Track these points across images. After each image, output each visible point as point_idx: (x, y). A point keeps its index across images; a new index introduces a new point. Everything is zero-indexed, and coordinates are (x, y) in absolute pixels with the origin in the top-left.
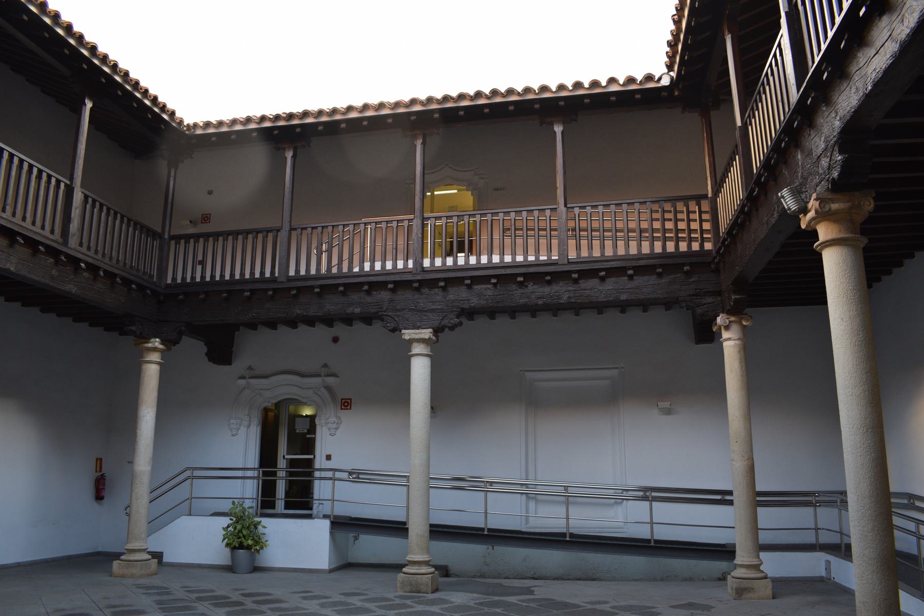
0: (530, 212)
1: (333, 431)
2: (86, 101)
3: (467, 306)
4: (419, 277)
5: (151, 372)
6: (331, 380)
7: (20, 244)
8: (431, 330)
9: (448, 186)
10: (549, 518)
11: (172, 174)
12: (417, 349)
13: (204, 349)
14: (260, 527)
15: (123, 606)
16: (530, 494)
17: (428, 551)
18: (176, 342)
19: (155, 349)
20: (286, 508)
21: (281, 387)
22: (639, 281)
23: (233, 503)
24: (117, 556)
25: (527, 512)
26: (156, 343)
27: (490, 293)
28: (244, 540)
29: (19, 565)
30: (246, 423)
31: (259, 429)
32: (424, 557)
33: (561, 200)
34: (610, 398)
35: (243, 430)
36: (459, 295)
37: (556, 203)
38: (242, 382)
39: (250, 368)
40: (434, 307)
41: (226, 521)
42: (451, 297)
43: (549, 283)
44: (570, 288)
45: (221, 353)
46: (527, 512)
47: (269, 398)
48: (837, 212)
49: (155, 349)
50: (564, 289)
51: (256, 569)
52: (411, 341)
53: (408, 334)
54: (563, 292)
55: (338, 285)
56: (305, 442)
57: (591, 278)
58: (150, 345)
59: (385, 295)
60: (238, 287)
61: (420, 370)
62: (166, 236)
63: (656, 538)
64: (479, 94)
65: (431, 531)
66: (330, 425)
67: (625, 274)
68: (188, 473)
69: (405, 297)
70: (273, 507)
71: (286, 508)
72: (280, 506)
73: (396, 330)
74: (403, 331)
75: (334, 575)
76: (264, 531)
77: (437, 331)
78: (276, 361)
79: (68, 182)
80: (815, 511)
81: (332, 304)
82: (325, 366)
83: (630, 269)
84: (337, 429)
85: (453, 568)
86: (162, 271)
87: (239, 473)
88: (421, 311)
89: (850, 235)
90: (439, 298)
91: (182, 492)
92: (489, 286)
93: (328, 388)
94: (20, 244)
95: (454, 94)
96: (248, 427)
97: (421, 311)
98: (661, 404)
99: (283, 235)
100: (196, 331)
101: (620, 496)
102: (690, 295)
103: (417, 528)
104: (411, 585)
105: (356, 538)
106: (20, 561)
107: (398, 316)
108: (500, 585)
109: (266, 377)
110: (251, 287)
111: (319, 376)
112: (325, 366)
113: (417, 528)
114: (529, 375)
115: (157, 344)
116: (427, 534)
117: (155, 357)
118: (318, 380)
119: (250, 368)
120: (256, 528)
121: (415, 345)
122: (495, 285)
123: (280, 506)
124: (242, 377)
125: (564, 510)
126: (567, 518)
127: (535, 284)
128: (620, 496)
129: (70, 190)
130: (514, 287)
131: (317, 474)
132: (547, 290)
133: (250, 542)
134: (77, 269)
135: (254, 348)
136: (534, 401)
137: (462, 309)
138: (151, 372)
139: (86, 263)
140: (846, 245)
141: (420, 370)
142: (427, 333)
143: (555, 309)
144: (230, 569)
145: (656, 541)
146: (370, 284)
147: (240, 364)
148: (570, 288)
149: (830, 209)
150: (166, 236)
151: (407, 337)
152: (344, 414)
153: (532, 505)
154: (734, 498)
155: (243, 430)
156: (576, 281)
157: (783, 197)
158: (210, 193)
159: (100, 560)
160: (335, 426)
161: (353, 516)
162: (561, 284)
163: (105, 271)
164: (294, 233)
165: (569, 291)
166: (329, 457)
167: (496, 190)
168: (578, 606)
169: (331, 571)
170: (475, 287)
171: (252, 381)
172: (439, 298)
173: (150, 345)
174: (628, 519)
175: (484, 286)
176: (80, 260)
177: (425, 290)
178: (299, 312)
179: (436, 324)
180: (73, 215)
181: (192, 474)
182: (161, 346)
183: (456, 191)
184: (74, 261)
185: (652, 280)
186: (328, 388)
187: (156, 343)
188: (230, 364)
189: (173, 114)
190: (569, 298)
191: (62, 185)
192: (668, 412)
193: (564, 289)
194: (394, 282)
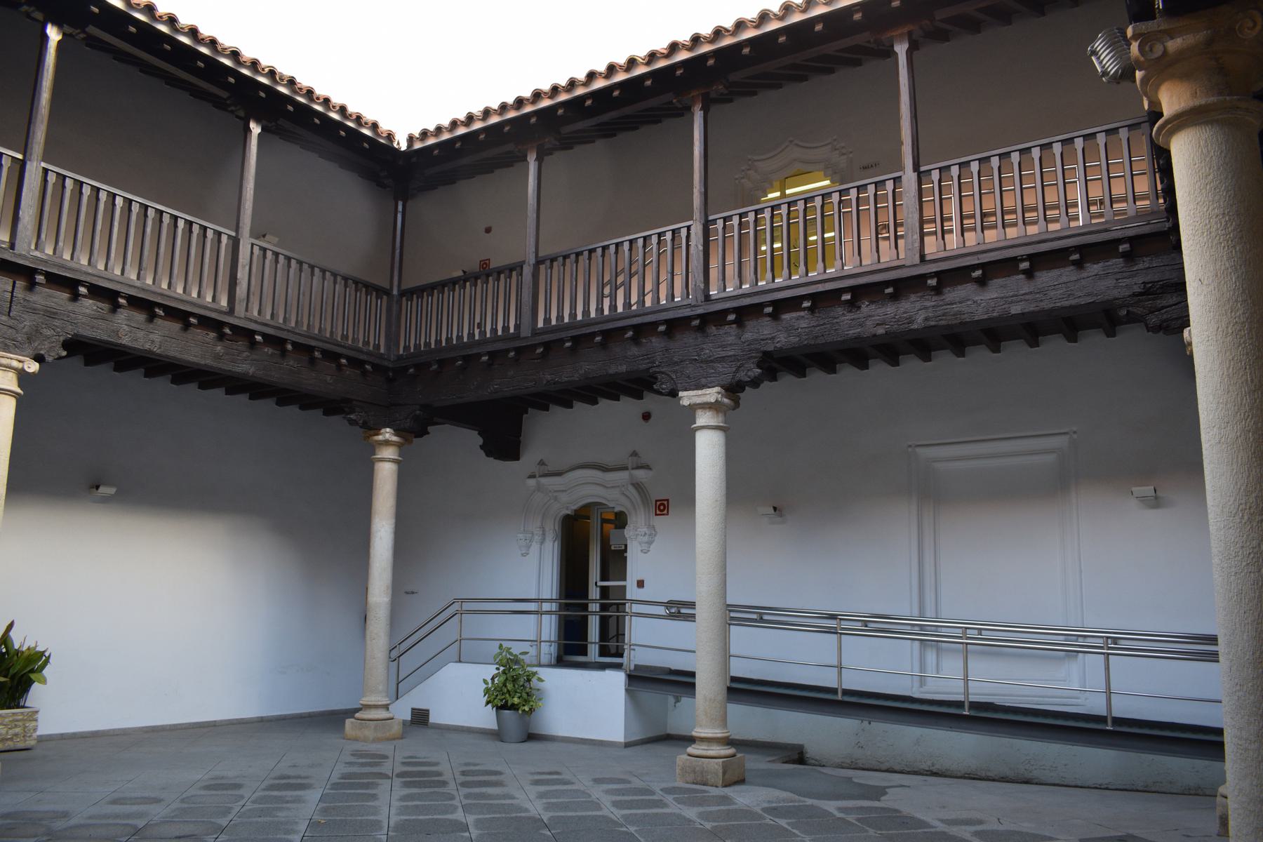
0: (861, 189)
1: (645, 547)
2: (252, 125)
3: (770, 348)
4: (700, 311)
5: (386, 474)
6: (641, 474)
7: (161, 317)
8: (717, 389)
9: (801, 175)
10: (945, 679)
11: (400, 208)
12: (703, 418)
13: (480, 441)
14: (534, 680)
15: (299, 777)
16: (926, 635)
17: (724, 722)
18: (422, 432)
19: (387, 443)
20: (602, 654)
21: (581, 489)
22: (1045, 278)
23: (501, 646)
24: (351, 713)
25: (923, 667)
26: (387, 434)
27: (803, 324)
28: (513, 694)
29: (261, 720)
30: (537, 538)
31: (557, 546)
32: (718, 733)
33: (908, 162)
34: (1057, 483)
35: (535, 547)
36: (764, 333)
37: (902, 168)
38: (532, 482)
39: (542, 463)
40: (723, 354)
41: (491, 670)
42: (748, 336)
43: (895, 297)
44: (928, 304)
45: (504, 443)
46: (923, 667)
47: (569, 502)
48: (1181, 55)
49: (387, 443)
50: (918, 305)
51: (531, 737)
52: (693, 408)
53: (688, 397)
54: (917, 312)
55: (594, 334)
56: (615, 562)
57: (961, 284)
58: (380, 438)
59: (656, 343)
60: (475, 351)
61: (708, 450)
62: (395, 292)
63: (1114, 714)
64: (764, 17)
65: (730, 690)
66: (640, 538)
67: (1017, 271)
68: (456, 607)
69: (687, 342)
70: (584, 651)
71: (602, 654)
72: (593, 652)
73: (674, 394)
74: (681, 394)
75: (629, 751)
76: (541, 685)
77: (733, 389)
78: (576, 451)
79: (233, 234)
80: (967, 693)
81: (589, 366)
82: (634, 454)
83: (1023, 260)
84: (650, 543)
85: (812, 751)
86: (392, 339)
87: (532, 607)
88: (706, 362)
89: (1212, 99)
90: (731, 339)
91: (450, 632)
92: (802, 314)
93: (638, 486)
94: (161, 317)
95: (728, 24)
96: (542, 543)
97: (706, 362)
98: (1138, 490)
99: (527, 271)
100: (461, 415)
101: (1071, 645)
102: (1134, 295)
103: (708, 685)
104: (694, 772)
105: (678, 700)
106: (264, 715)
107: (675, 372)
108: (849, 779)
109: (559, 474)
110: (490, 348)
111: (625, 468)
112: (634, 454)
113: (708, 685)
114: (924, 453)
115: (387, 436)
116: (723, 693)
117: (389, 453)
118: (624, 475)
119: (542, 463)
120: (529, 680)
121: (699, 413)
122: (811, 310)
123: (593, 652)
124: (532, 476)
125: (960, 664)
126: (966, 680)
127: (872, 302)
128: (1071, 645)
129: (235, 243)
130: (840, 310)
131: (554, 607)
132: (890, 310)
133: (516, 700)
134: (253, 344)
135: (548, 433)
136: (931, 493)
137: (766, 353)
138: (386, 474)
139: (264, 335)
140: (1206, 123)
141: (708, 450)
142: (712, 394)
143: (922, 344)
144: (497, 735)
145: (1118, 721)
146: (636, 328)
147: (529, 458)
148: (928, 304)
149: (1165, 52)
150: (395, 292)
151: (685, 402)
152: (659, 521)
153: (931, 656)
154: (1221, 648)
155: (535, 547)
156: (938, 290)
157: (1094, 53)
158: (488, 230)
159: (333, 720)
160: (646, 539)
161: (673, 668)
162: (913, 297)
163: (294, 344)
164: (542, 267)
165: (926, 308)
166: (641, 584)
167: (865, 168)
168: (922, 824)
169: (628, 745)
170: (786, 316)
171: (544, 480)
172: (731, 339)
173: (380, 438)
174: (1072, 685)
175: (794, 315)
176: (253, 332)
177: (713, 330)
178: (549, 377)
179: (727, 379)
180: (239, 275)
181: (461, 608)
182: (395, 438)
183: (827, 182)
184: (248, 334)
185: (1067, 274)
186: (638, 486)
187: (387, 434)
188: (517, 458)
189: (375, 126)
190: (926, 319)
191: (224, 239)
192: (1155, 502)
193: (918, 305)
194: (667, 322)
